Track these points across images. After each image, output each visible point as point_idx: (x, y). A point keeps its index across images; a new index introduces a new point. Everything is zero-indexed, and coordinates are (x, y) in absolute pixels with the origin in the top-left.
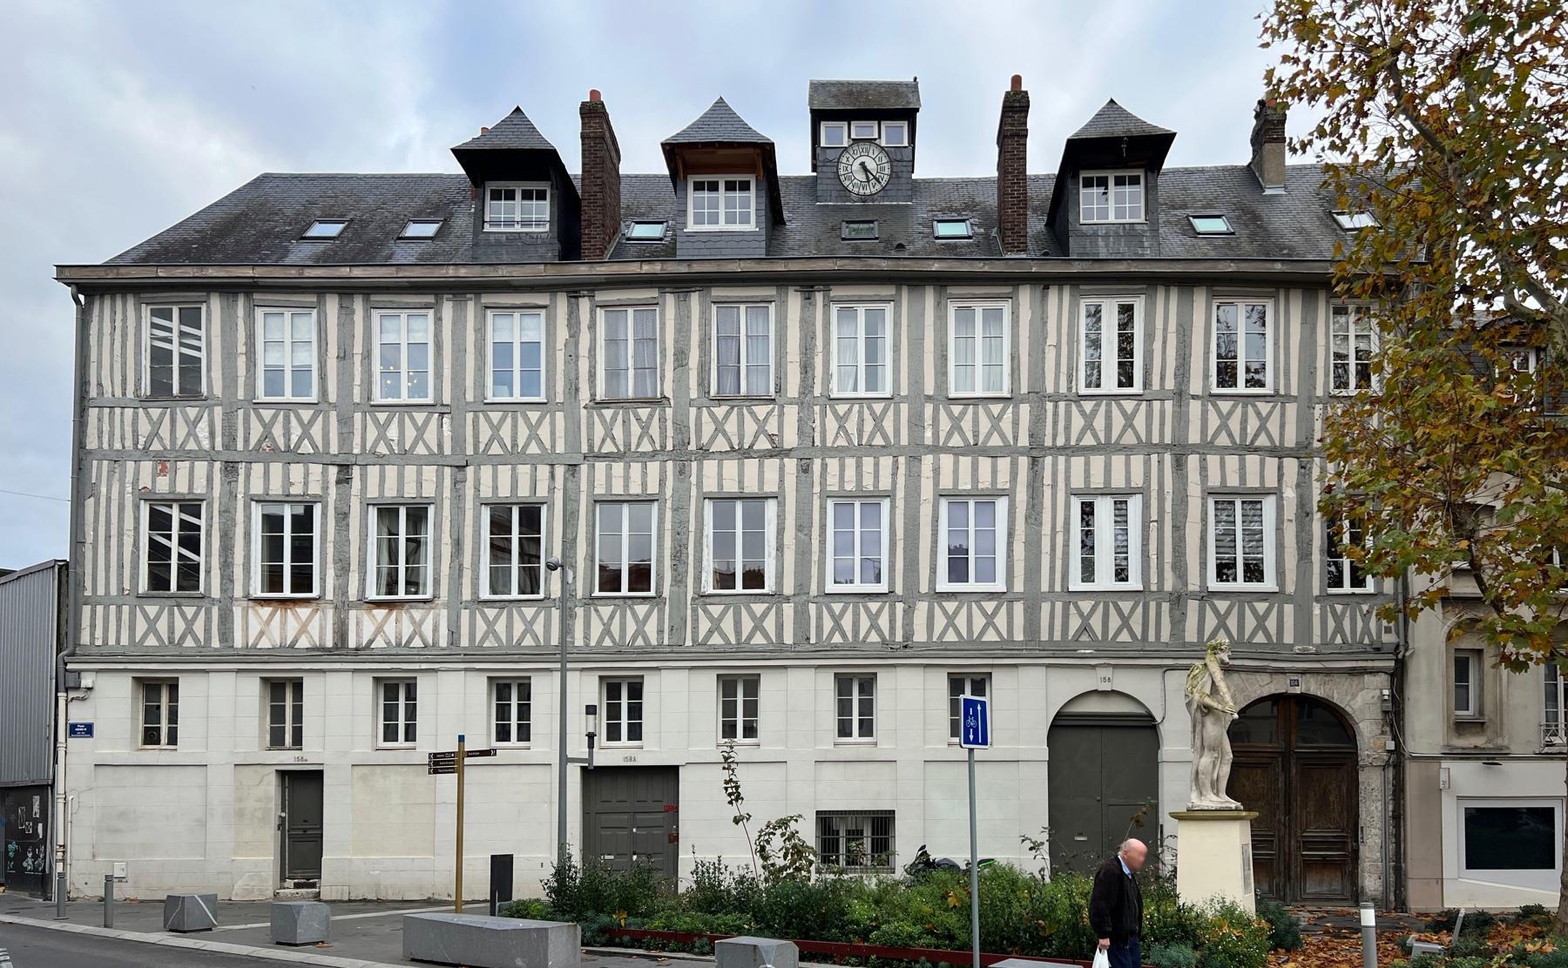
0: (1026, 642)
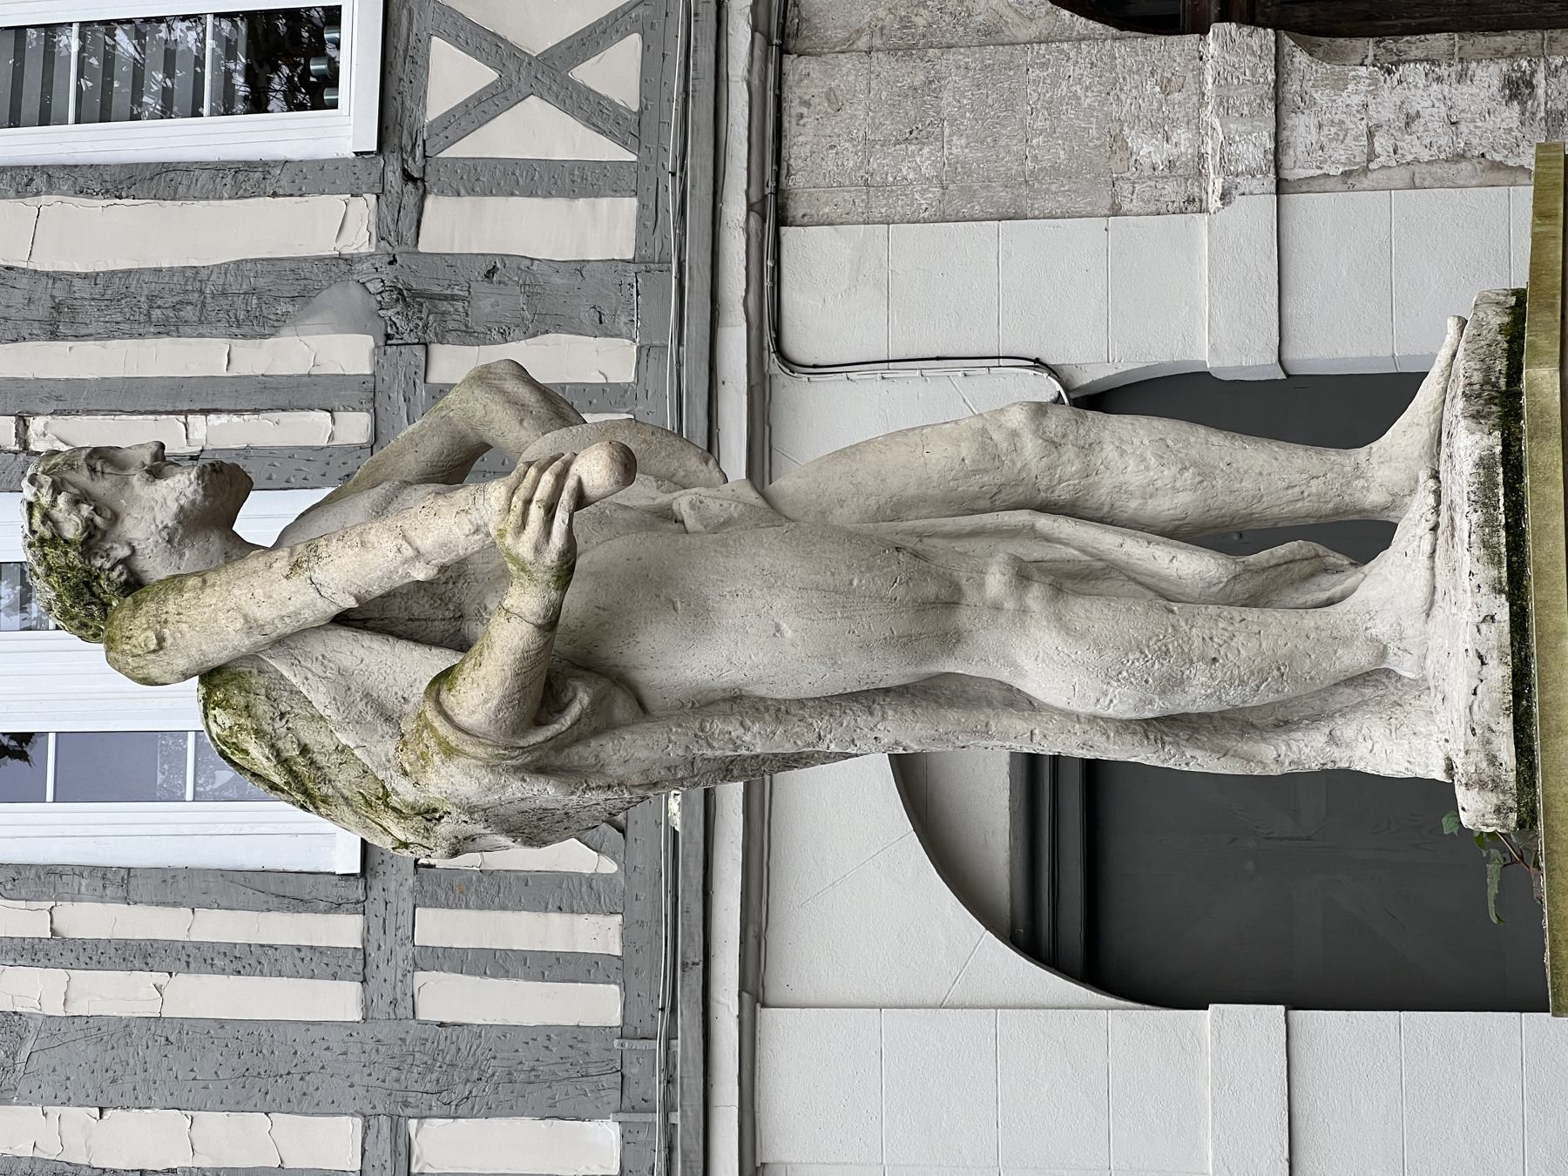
0: (627, 1107)
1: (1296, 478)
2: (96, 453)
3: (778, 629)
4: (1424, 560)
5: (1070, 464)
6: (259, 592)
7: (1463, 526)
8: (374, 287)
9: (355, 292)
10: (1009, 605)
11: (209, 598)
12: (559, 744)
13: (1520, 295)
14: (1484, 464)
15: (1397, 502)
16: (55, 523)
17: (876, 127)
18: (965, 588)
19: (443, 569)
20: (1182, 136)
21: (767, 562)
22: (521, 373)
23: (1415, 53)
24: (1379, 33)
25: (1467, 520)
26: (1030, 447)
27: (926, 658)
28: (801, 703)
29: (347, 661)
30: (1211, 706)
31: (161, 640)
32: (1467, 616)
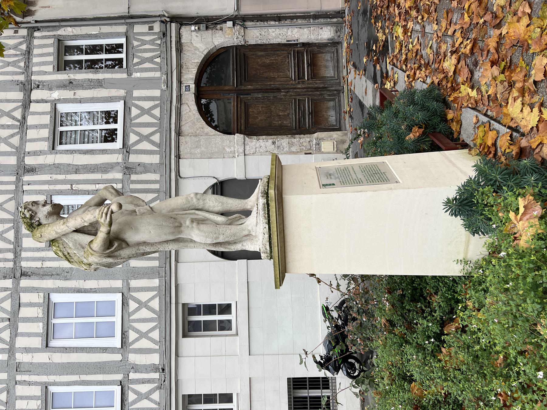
1: (237, 204)
2: (34, 202)
3: (150, 232)
4: (255, 218)
5: (201, 203)
6: (58, 228)
7: (261, 213)
8: (122, 167)
9: (120, 168)
10: (190, 226)
11: (50, 228)
12: (112, 252)
13: (269, 176)
14: (264, 204)
15: (252, 207)
16: (25, 215)
17: (192, 146)
18: (183, 224)
19: (90, 223)
20: (232, 148)
21: (148, 221)
22: (113, 187)
23: (261, 138)
24: (257, 136)
25: (261, 213)
26: (195, 200)
27: (177, 235)
28: (156, 243)
29: (76, 238)
30: (224, 241)
31: (41, 236)
32: (262, 227)
